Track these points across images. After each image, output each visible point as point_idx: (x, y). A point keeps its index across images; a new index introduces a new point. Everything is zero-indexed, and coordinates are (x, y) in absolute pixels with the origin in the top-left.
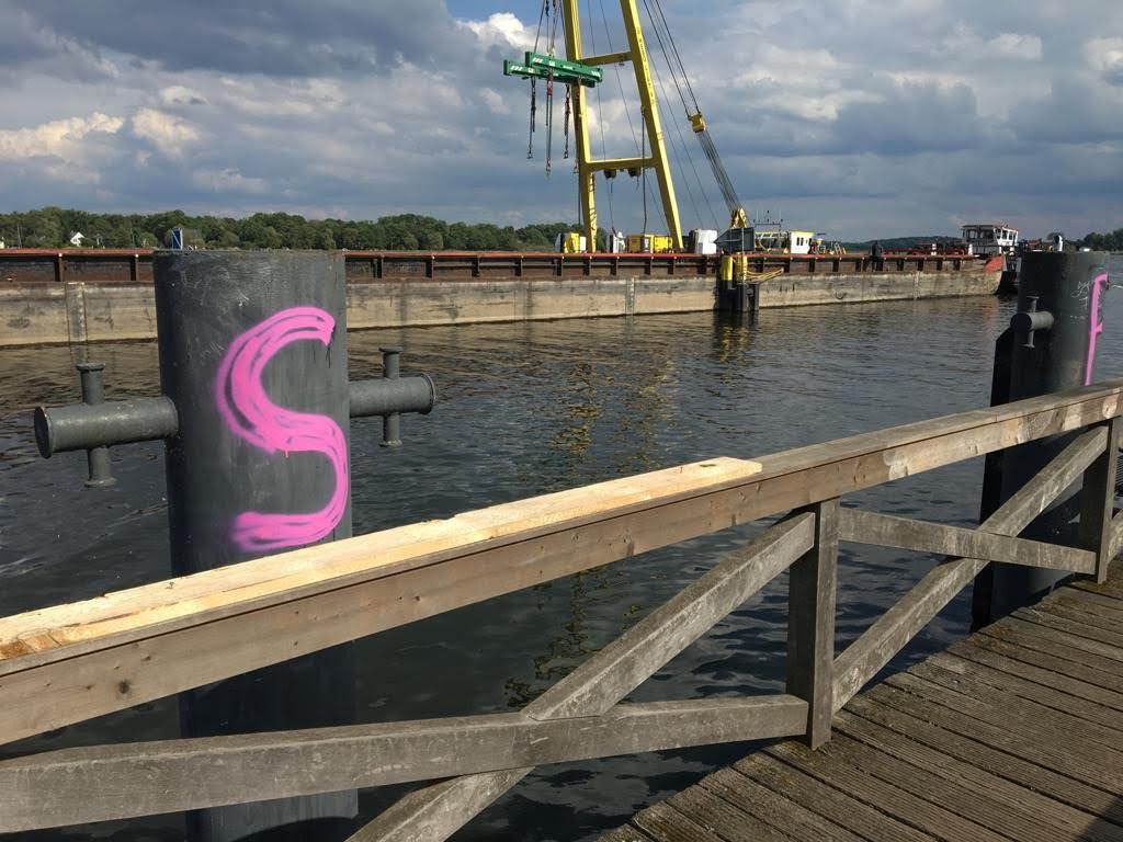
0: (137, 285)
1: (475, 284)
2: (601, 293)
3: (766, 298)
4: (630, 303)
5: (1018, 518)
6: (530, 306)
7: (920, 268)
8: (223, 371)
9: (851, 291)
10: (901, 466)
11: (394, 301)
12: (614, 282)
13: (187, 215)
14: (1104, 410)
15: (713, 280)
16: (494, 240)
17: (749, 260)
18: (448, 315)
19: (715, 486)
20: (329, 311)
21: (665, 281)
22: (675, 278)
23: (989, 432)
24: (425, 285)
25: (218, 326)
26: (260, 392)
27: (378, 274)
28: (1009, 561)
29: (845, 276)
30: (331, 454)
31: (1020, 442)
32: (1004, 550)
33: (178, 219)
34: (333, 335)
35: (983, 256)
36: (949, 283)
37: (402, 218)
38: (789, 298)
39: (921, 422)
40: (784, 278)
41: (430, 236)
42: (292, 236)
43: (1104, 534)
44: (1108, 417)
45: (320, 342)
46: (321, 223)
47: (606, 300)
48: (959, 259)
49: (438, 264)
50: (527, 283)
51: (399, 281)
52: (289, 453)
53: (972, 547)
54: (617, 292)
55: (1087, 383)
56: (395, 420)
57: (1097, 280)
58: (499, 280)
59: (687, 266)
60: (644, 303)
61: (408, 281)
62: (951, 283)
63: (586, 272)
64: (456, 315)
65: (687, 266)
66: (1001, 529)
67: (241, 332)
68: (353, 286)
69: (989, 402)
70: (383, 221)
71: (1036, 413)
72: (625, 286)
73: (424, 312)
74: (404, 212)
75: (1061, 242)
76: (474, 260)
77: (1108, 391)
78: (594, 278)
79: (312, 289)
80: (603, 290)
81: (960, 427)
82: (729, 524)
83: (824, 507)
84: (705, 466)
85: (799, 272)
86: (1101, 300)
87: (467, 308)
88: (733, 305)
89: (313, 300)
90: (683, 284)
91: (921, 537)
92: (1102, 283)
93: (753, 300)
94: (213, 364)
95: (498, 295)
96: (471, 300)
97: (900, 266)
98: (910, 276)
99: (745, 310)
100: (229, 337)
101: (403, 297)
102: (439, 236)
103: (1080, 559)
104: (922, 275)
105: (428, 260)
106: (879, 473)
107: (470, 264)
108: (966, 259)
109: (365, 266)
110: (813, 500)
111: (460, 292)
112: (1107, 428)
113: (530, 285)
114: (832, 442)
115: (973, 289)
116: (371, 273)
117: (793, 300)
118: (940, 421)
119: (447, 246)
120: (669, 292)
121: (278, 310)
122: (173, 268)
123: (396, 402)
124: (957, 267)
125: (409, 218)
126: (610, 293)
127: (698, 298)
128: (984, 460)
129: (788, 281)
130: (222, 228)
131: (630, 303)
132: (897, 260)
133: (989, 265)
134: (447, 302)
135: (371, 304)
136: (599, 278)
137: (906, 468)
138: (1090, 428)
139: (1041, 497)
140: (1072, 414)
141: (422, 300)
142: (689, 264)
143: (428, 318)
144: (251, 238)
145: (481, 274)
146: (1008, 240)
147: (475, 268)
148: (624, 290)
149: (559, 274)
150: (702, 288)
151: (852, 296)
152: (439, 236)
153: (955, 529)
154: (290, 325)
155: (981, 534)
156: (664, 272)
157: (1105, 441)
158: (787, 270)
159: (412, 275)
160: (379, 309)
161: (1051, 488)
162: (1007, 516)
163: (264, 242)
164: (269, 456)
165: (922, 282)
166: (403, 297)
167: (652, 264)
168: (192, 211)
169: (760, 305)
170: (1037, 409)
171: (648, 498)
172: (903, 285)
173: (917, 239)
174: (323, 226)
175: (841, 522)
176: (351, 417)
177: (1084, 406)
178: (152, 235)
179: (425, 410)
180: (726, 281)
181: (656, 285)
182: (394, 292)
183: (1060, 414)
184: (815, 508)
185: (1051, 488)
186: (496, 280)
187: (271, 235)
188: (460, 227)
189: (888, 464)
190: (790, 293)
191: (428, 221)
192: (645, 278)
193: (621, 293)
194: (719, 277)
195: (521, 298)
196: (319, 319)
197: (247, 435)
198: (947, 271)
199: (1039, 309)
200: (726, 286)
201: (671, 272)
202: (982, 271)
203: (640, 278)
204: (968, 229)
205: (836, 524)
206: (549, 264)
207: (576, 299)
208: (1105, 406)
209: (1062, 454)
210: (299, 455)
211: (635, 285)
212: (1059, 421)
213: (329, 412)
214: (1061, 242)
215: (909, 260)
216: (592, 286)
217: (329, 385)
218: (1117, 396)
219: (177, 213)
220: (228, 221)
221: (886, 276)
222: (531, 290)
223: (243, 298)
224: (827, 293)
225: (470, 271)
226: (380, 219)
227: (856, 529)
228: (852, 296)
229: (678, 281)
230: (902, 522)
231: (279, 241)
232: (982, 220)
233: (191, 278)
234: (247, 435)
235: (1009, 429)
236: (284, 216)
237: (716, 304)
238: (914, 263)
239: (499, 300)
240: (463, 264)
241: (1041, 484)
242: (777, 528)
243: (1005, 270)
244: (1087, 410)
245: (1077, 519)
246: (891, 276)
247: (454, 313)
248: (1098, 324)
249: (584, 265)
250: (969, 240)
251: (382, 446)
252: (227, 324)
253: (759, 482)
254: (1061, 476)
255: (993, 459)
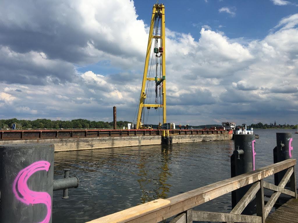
0: (2, 140)
1: (98, 138)
2: (132, 140)
3: (174, 141)
4: (140, 143)
5: (240, 209)
6: (113, 144)
7: (213, 133)
8: (15, 181)
9: (196, 139)
10: (208, 198)
11: (75, 143)
12: (135, 137)
13: (17, 119)
14: (258, 178)
15: (161, 136)
16: (103, 125)
17: (169, 131)
18: (90, 146)
19: (157, 209)
20: (49, 161)
21: (149, 137)
22: (152, 136)
23: (230, 186)
24: (84, 139)
25: (15, 167)
26: (26, 186)
27: (71, 136)
28: (239, 222)
29: (194, 135)
30: (47, 204)
31: (238, 188)
32: (237, 219)
33: (15, 120)
34: (49, 168)
35: (228, 130)
36: (220, 137)
37: (78, 120)
38: (181, 141)
39: (212, 184)
40: (179, 136)
41: (86, 125)
42: (47, 125)
43: (263, 212)
44: (260, 179)
45: (45, 171)
46: (55, 121)
47: (134, 142)
48: (222, 131)
49: (88, 133)
50: (112, 138)
51: (77, 138)
52: (33, 204)
53: (229, 219)
54: (136, 140)
55: (254, 170)
56: (67, 190)
57: (253, 142)
58: (105, 137)
59: (154, 133)
60: (144, 142)
61: (79, 138)
62: (221, 137)
63: (128, 135)
64: (93, 147)
65: (154, 133)
66: (236, 213)
67: (22, 169)
68: (64, 139)
69: (230, 176)
70: (73, 121)
71: (241, 180)
72: (139, 138)
73: (84, 146)
74: (79, 118)
75: (246, 127)
76: (98, 132)
77: (259, 172)
78: (130, 136)
79: (44, 156)
80: (132, 139)
81: (222, 186)
82: (161, 220)
83: (188, 212)
84: (155, 202)
85: (183, 134)
86: (255, 146)
87: (96, 145)
88: (166, 143)
89: (44, 159)
90: (153, 138)
91: (215, 217)
92: (254, 142)
93: (171, 141)
94: (13, 178)
95: (104, 141)
96: (96, 142)
97: (208, 133)
98: (210, 135)
99: (169, 144)
100: (19, 170)
101: (78, 142)
102: (88, 124)
103: (257, 219)
104: (213, 135)
105: (85, 132)
106: (202, 201)
107: (97, 133)
108: (223, 131)
109: (67, 134)
110: (185, 210)
111: (94, 140)
112: (260, 182)
113: (113, 138)
114: (189, 192)
115: (226, 139)
116: (69, 136)
117: (182, 141)
118: (217, 184)
119: (90, 127)
120: (150, 140)
121: (33, 162)
122: (4, 151)
123: (67, 185)
124: (222, 133)
125: (80, 120)
126: (135, 140)
127: (157, 141)
128: (231, 193)
129: (180, 137)
130: (27, 123)
131: (140, 143)
132: (207, 131)
133: (229, 132)
134: (90, 143)
135: (69, 144)
136: (132, 136)
137: (209, 198)
138: (255, 183)
139: (245, 203)
140: (251, 179)
141: (83, 143)
142: (154, 132)
143: (84, 148)
144: (35, 126)
145: (100, 136)
146: (233, 126)
147: (98, 134)
148: (138, 139)
149: (121, 135)
150: (158, 138)
151: (197, 140)
152: (88, 124)
153: (224, 214)
154: (39, 166)
155: (230, 215)
156: (148, 134)
157: (260, 185)
158: (180, 134)
159: (81, 136)
160: (71, 146)
161: (247, 200)
162: (237, 209)
163: (39, 127)
164: (27, 206)
165: (213, 137)
166: (78, 142)
167: (145, 132)
168: (19, 119)
169: (173, 143)
170: (241, 179)
171: (138, 214)
172: (209, 137)
173: (211, 125)
174: (56, 122)
175: (193, 216)
176: (53, 191)
177: (253, 177)
178: (7, 125)
179: (76, 187)
180: (164, 137)
181: (147, 138)
182: (76, 141)
183: (247, 179)
184: (186, 212)
185: (247, 200)
186: (104, 137)
187: (41, 125)
188: (94, 122)
189: (204, 197)
190: (181, 140)
191: (85, 120)
192: (144, 136)
193: (137, 140)
194: (162, 135)
195: (111, 142)
196: (46, 164)
197: (20, 199)
198: (219, 134)
199: (240, 149)
200: (164, 138)
201: (150, 134)
202: (228, 134)
203: (142, 136)
204: (223, 123)
205: (192, 216)
206: (118, 133)
207: (125, 142)
208: (258, 176)
209: (250, 190)
210: (36, 205)
211: (141, 138)
212: (247, 182)
213: (47, 191)
214: (246, 127)
215: (210, 131)
216: (129, 138)
217: (47, 183)
218: (261, 174)
219: (15, 119)
220: (29, 121)
221: (204, 135)
222: (113, 140)
223: (23, 159)
224: (190, 140)
225: (97, 135)
226: (72, 120)
227: (197, 217)
228: (197, 140)
229: (152, 136)
230: (210, 214)
231: (43, 127)
232: (226, 121)
233: (9, 154)
234: (20, 199)
235: (234, 185)
236: (45, 120)
237: (161, 143)
238: (211, 132)
239: (105, 142)
240: (95, 133)
241: (245, 199)
242: (176, 219)
243: (233, 133)
244: (254, 178)
245: (256, 206)
246: (206, 135)
247: (92, 146)
248: (255, 153)
249: (128, 133)
250: (224, 126)
251: (62, 198)
252: (18, 167)
253: (170, 206)
254: (250, 196)
255: (234, 193)
